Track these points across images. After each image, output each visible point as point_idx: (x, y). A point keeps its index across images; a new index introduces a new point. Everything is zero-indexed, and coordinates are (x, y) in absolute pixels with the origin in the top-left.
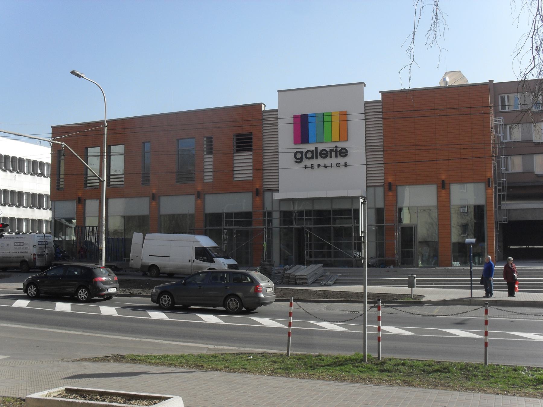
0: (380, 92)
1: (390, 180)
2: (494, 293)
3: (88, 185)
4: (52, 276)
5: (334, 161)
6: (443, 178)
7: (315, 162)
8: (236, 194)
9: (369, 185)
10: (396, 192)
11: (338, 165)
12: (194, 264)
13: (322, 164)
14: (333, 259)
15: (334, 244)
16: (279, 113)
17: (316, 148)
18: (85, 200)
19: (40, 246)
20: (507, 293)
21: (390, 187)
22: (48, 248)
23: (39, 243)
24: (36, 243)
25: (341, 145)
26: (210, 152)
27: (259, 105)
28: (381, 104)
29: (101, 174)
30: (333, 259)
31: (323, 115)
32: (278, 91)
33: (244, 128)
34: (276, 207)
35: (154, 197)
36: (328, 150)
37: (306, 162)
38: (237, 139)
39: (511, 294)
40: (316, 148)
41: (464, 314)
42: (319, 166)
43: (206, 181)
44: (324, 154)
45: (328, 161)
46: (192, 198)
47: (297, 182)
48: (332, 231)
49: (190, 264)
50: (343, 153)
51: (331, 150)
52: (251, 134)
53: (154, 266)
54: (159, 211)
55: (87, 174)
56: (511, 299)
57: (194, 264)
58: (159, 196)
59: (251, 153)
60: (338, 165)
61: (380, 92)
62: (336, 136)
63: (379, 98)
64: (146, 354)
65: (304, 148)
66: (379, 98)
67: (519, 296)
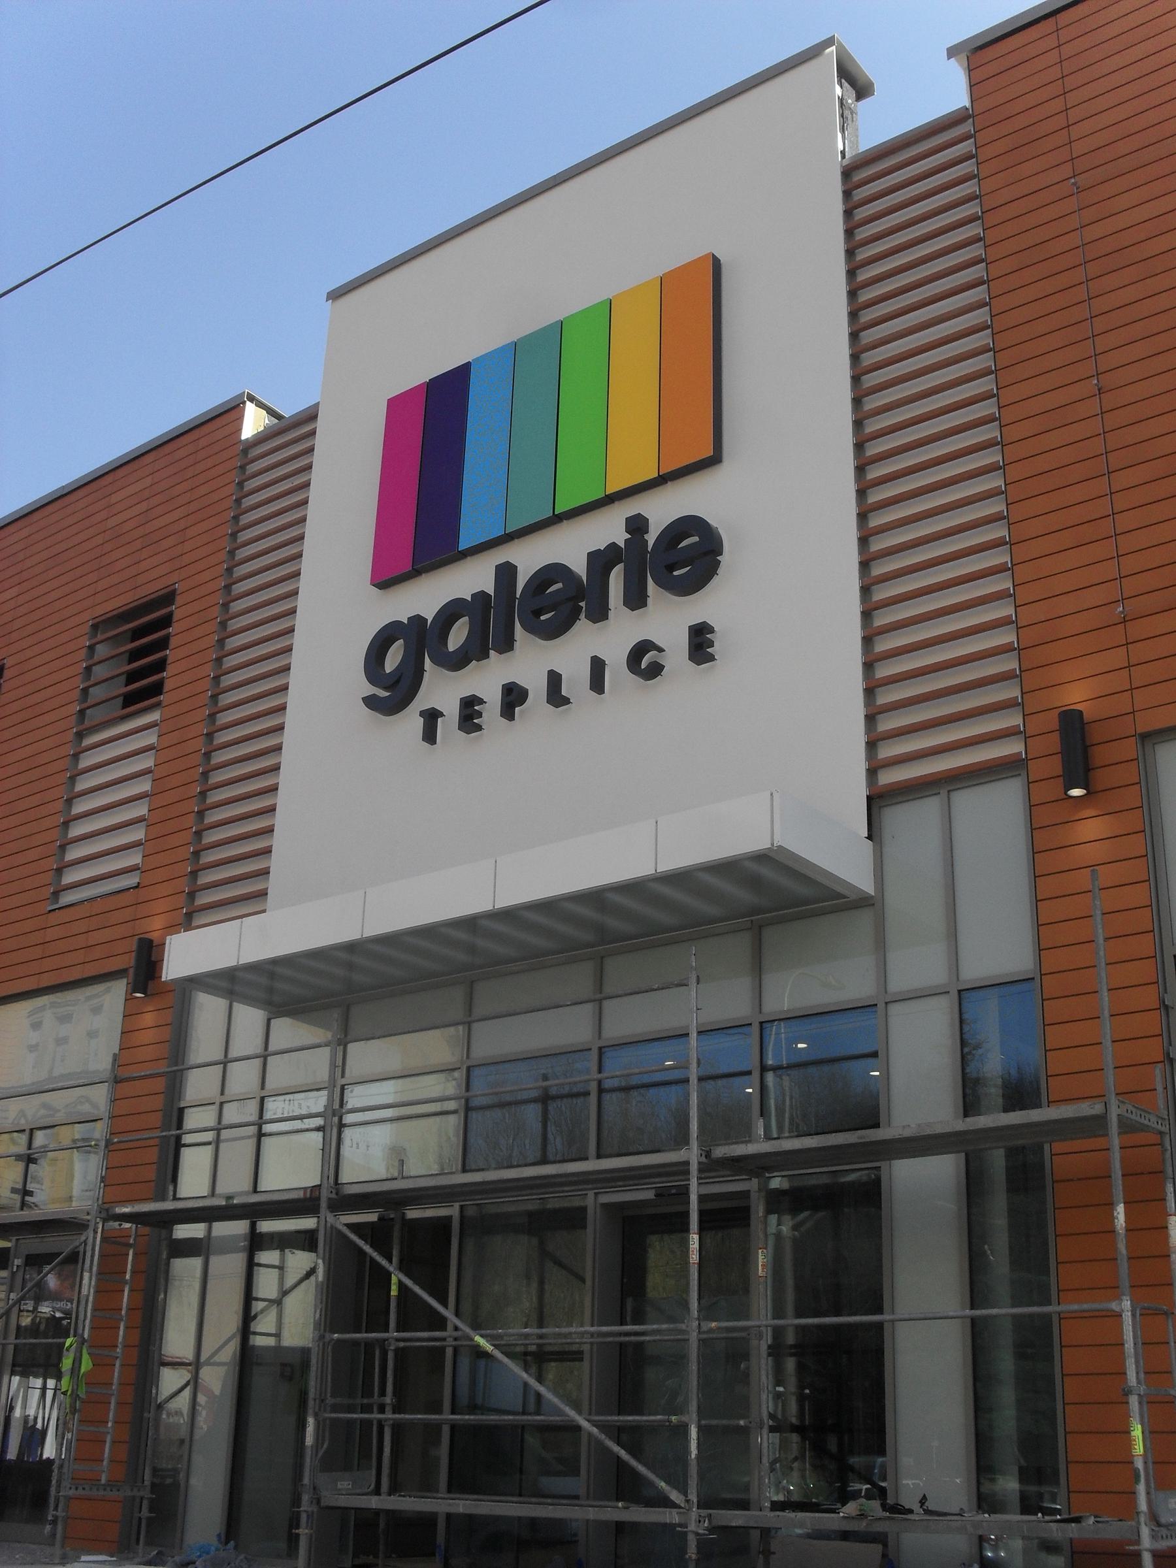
0: (952, 52)
4: (61, 1300)
7: (486, 680)
11: (644, 661)
14: (1116, 1142)
15: (439, 1323)
16: (321, 425)
29: (154, 725)
30: (1116, 1142)
31: (554, 336)
36: (579, 567)
37: (442, 690)
42: (513, 697)
44: (559, 602)
48: (396, 1234)
50: (689, 557)
51: (602, 561)
60: (644, 661)
61: (952, 52)
63: (950, 92)
64: (844, 1544)
65: (425, 598)
66: (950, 92)
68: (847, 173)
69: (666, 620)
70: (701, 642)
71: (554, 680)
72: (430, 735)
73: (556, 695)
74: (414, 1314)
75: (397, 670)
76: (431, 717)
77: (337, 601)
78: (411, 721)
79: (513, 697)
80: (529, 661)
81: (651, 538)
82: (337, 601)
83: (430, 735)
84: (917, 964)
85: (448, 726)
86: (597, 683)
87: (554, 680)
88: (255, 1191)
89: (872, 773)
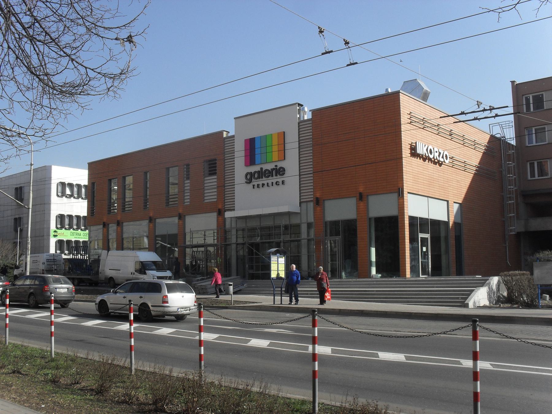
1: (318, 195)
2: (220, 296)
3: (170, 203)
5: (274, 179)
6: (361, 190)
7: (260, 182)
8: (343, 200)
9: (302, 200)
10: (324, 207)
11: (277, 183)
12: (134, 276)
13: (270, 182)
14: (260, 272)
16: (235, 138)
17: (262, 169)
18: (185, 216)
19: (49, 263)
20: (319, 300)
21: (318, 202)
22: (56, 265)
23: (48, 260)
24: (45, 261)
25: (280, 164)
26: (188, 178)
27: (221, 133)
28: (311, 122)
30: (260, 272)
32: (235, 118)
33: (206, 157)
34: (234, 225)
35: (361, 197)
37: (255, 182)
38: (209, 164)
39: (323, 301)
40: (262, 169)
41: (288, 319)
43: (206, 201)
45: (270, 180)
46: (145, 223)
47: (252, 202)
49: (132, 276)
52: (216, 160)
53: (111, 278)
54: (155, 231)
55: (168, 193)
56: (293, 305)
57: (134, 276)
58: (368, 196)
59: (216, 177)
60: (277, 183)
62: (275, 156)
67: (331, 304)
68: (299, 123)
69: (280, 179)
70: (283, 182)
71: (268, 183)
72: (254, 188)
73: (268, 186)
74: (257, 254)
75: (250, 178)
76: (254, 186)
77: (240, 169)
78: (251, 185)
79: (263, 185)
80: (264, 181)
81: (278, 168)
82: (240, 169)
83: (254, 188)
84: (304, 220)
85: (256, 186)
86: (272, 185)
87: (268, 183)
88: (281, 304)
89: (300, 200)
